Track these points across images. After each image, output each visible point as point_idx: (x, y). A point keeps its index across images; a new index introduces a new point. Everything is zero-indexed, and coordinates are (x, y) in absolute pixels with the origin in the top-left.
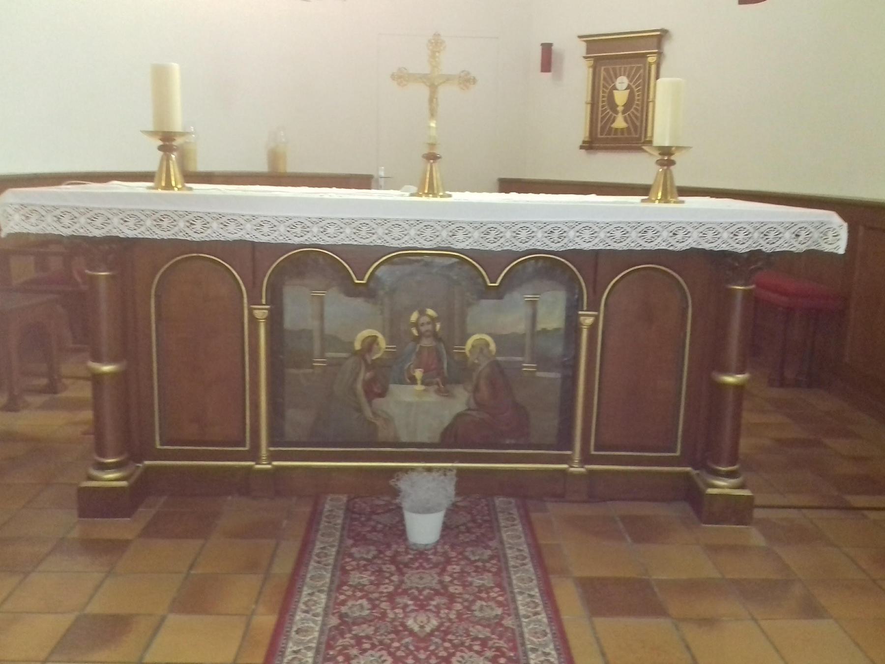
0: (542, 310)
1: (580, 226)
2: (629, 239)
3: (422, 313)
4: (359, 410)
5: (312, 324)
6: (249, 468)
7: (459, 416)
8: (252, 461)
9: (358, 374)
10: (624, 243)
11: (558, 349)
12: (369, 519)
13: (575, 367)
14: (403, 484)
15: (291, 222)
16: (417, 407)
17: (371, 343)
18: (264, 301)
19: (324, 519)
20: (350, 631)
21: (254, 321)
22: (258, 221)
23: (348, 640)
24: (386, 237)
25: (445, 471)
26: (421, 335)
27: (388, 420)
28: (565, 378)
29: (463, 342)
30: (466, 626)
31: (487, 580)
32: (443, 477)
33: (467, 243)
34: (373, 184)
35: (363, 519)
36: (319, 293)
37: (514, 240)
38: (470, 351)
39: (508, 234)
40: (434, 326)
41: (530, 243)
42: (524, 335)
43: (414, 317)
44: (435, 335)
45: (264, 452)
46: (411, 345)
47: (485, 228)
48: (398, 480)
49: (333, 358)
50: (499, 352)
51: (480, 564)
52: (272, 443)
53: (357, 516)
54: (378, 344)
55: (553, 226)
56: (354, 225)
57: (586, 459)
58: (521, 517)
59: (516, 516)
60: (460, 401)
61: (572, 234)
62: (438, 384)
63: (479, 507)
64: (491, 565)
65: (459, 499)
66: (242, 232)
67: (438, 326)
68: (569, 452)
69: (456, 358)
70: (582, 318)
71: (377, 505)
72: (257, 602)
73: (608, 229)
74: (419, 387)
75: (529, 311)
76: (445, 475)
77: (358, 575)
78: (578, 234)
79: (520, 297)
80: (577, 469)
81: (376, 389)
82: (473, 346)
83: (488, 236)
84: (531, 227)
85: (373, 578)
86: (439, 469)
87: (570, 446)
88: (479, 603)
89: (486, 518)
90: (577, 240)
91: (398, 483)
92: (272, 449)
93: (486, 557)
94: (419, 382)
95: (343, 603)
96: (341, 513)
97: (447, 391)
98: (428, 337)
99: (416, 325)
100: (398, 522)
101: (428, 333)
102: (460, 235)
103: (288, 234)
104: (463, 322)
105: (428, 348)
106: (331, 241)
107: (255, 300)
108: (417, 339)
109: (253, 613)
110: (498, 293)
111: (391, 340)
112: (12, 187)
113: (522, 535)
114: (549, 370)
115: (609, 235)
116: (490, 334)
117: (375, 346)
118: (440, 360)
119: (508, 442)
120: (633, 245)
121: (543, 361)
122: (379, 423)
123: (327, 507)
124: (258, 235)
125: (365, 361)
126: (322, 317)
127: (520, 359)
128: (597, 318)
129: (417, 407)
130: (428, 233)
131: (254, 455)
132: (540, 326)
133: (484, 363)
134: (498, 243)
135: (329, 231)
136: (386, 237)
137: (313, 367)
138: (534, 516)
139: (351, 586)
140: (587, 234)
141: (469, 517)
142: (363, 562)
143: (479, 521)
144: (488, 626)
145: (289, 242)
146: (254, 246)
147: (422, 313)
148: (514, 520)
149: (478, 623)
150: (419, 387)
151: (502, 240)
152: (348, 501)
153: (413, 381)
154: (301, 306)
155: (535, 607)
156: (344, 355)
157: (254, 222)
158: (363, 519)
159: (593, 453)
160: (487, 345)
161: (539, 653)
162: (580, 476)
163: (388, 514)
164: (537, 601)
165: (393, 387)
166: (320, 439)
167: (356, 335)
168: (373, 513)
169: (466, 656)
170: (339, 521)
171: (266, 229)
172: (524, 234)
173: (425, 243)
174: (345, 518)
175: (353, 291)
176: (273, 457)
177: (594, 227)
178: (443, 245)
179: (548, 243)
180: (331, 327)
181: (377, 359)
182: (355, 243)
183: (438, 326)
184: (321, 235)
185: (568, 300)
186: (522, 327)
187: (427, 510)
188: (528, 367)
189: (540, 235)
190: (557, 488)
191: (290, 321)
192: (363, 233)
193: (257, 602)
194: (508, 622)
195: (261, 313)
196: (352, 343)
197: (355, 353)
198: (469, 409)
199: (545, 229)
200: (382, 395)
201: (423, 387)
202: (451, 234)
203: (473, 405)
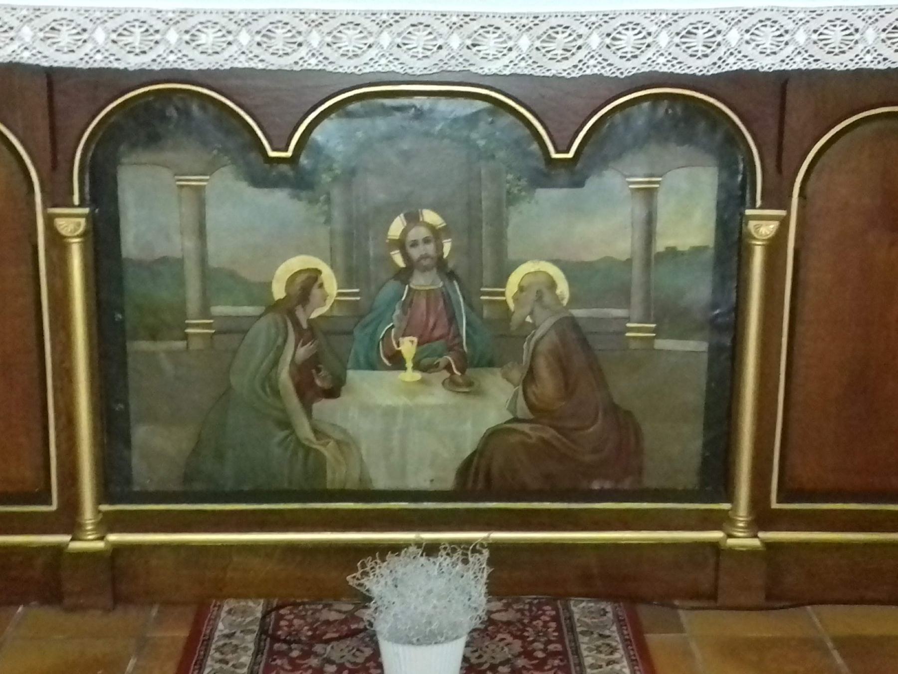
0: (666, 209)
1: (753, 20)
2: (860, 46)
3: (413, 219)
4: (286, 424)
5: (181, 245)
6: (58, 550)
7: (493, 434)
8: (66, 532)
9: (280, 350)
10: (850, 55)
11: (699, 290)
12: (306, 654)
13: (735, 326)
14: (377, 582)
15: (119, 21)
16: (406, 419)
17: (306, 286)
18: (76, 199)
19: (214, 654)
21: (57, 242)
22: (48, 19)
24: (327, 51)
25: (466, 549)
26: (411, 267)
27: (346, 444)
28: (715, 351)
29: (502, 280)
32: (460, 567)
33: (506, 61)
35: (295, 654)
36: (194, 181)
37: (606, 53)
38: (516, 299)
39: (595, 40)
40: (439, 248)
41: (643, 58)
42: (629, 262)
43: (396, 228)
44: (440, 264)
45: (88, 515)
46: (392, 287)
47: (544, 27)
48: (365, 574)
49: (228, 317)
50: (575, 300)
52: (105, 494)
53: (284, 647)
54: (321, 286)
55: (693, 19)
56: (255, 27)
57: (762, 518)
58: (626, 642)
59: (616, 641)
60: (496, 403)
61: (733, 36)
62: (448, 367)
63: (539, 623)
65: (497, 605)
66: (14, 46)
67: (447, 247)
68: (726, 506)
69: (486, 313)
70: (752, 224)
71: (328, 623)
73: (813, 25)
74: (410, 375)
75: (640, 212)
76: (465, 561)
78: (747, 37)
79: (617, 184)
80: (742, 540)
81: (320, 381)
82: (521, 289)
83: (551, 46)
84: (645, 23)
86: (454, 546)
87: (727, 492)
89: (557, 647)
90: (748, 49)
91: (364, 581)
92: (105, 508)
94: (409, 364)
96: (250, 640)
97: (470, 384)
98: (425, 269)
99: (401, 244)
100: (368, 660)
101: (426, 263)
102: (490, 44)
103: (114, 49)
104: (499, 238)
105: (428, 292)
106: (206, 63)
107: (57, 196)
108: (404, 275)
110: (574, 174)
111: (349, 277)
112: (320, 259)
114: (682, 336)
115: (815, 37)
116: (556, 262)
117: (315, 291)
118: (453, 319)
119: (596, 486)
120: (868, 58)
121: (668, 316)
122: (328, 451)
123: (221, 627)
124: (50, 52)
125: (296, 323)
126: (201, 233)
127: (620, 312)
128: (784, 223)
129: (406, 419)
130: (420, 38)
132: (661, 245)
133: (546, 323)
134: (574, 61)
135: (203, 39)
136: (327, 51)
137: (186, 337)
138: (653, 639)
140: (767, 37)
141: (517, 645)
143: (540, 655)
145: (116, 65)
146: (52, 77)
147: (413, 219)
148: (613, 650)
150: (410, 375)
151: (581, 54)
152: (264, 617)
153: (397, 361)
154: (162, 206)
155: (611, 653)
157: (38, 23)
158: (295, 654)
159: (775, 505)
160: (553, 285)
161: (595, 636)
162: (752, 553)
163: (348, 642)
164: (614, 644)
165: (353, 376)
166: (201, 486)
167: (277, 267)
168: (317, 638)
170: (246, 659)
171: (65, 37)
172: (628, 40)
173: (413, 62)
174: (258, 652)
175: (265, 173)
176: (109, 523)
177: (783, 20)
178: (453, 66)
179: (683, 57)
180: (220, 254)
181: (320, 317)
182: (261, 66)
183: (447, 247)
184: (187, 49)
185: (722, 187)
187: (427, 636)
188: (638, 329)
189: (663, 39)
190: (704, 580)
191: (137, 236)
192: (278, 44)
195: (72, 223)
196: (268, 285)
197: (274, 307)
198: (516, 420)
199: (674, 28)
200: (332, 393)
201: (418, 376)
202: (469, 42)
203: (523, 410)
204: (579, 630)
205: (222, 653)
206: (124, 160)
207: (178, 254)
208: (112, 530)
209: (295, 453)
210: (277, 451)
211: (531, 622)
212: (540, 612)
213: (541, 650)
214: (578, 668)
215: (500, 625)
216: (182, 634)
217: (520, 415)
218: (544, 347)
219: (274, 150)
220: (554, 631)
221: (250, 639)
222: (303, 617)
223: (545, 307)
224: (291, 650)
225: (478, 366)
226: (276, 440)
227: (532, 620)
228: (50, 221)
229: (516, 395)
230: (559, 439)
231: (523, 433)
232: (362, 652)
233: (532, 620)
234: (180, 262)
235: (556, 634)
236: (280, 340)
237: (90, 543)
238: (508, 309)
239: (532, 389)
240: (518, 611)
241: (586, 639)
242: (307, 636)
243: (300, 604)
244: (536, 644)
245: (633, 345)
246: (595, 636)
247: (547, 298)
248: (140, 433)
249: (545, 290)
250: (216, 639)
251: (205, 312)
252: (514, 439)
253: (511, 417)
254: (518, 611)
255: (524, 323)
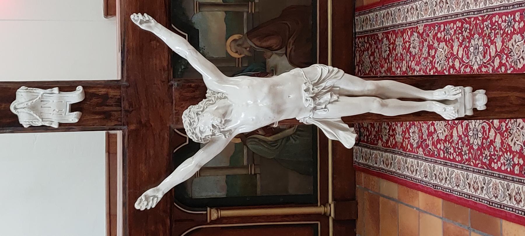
4: (288, 138)
9: (260, 140)
20: (425, 140)
21: (220, 220)
23: (429, 142)
30: (423, 59)
31: (399, 42)
34: (279, 70)
42: (226, 12)
45: (320, 210)
51: (391, 46)
59: (383, 12)
63: (503, 25)
64: (392, 38)
72: (413, 207)
77: (397, 136)
82: (237, 52)
85: (399, 125)
88: (411, 49)
93: (387, 43)
95: (412, 145)
109: (418, 209)
113: (376, 13)
116: (227, 40)
131: (324, 217)
139: (403, 140)
142: (391, 133)
144: (423, 43)
148: (412, 7)
149: (421, 50)
156: (245, 151)
158: (368, 134)
160: (235, 40)
161: (435, 8)
169: (437, 60)
176: (325, 202)
186: (220, 14)
193: (413, 207)
194: (421, 29)
195: (214, 214)
203: (283, 51)
204: (466, 9)
205: (521, 201)
206: (191, 196)
207: (225, 177)
208: (328, 202)
209: (299, 135)
210: (298, 142)
211: (503, 30)
212: (496, 24)
213: (519, 24)
214: (453, 17)
215: (504, 47)
216: (363, 175)
217: (284, 52)
218: (258, 43)
219: (186, 142)
220: (508, 17)
221: (512, 185)
222: (499, 157)
223: (243, 44)
224: (518, 164)
225: (265, 67)
226: (294, 142)
227: (501, 29)
228: (213, 222)
229: (276, 53)
230: (294, 37)
231: (291, 51)
232: (520, 124)
233: (501, 29)
234: (227, 176)
235: (509, 16)
236: (256, 140)
237: (331, 209)
238: (244, 57)
239: (274, 47)
240: (495, 37)
241: (409, 19)
242: (510, 155)
243: (491, 158)
244: (516, 27)
245: (257, 10)
246: (435, 8)
247: (240, 42)
248: (291, 191)
249: (238, 43)
250: (512, 205)
251: (246, 167)
252: (293, 53)
253: (285, 56)
254: (495, 37)
255: (249, 51)
